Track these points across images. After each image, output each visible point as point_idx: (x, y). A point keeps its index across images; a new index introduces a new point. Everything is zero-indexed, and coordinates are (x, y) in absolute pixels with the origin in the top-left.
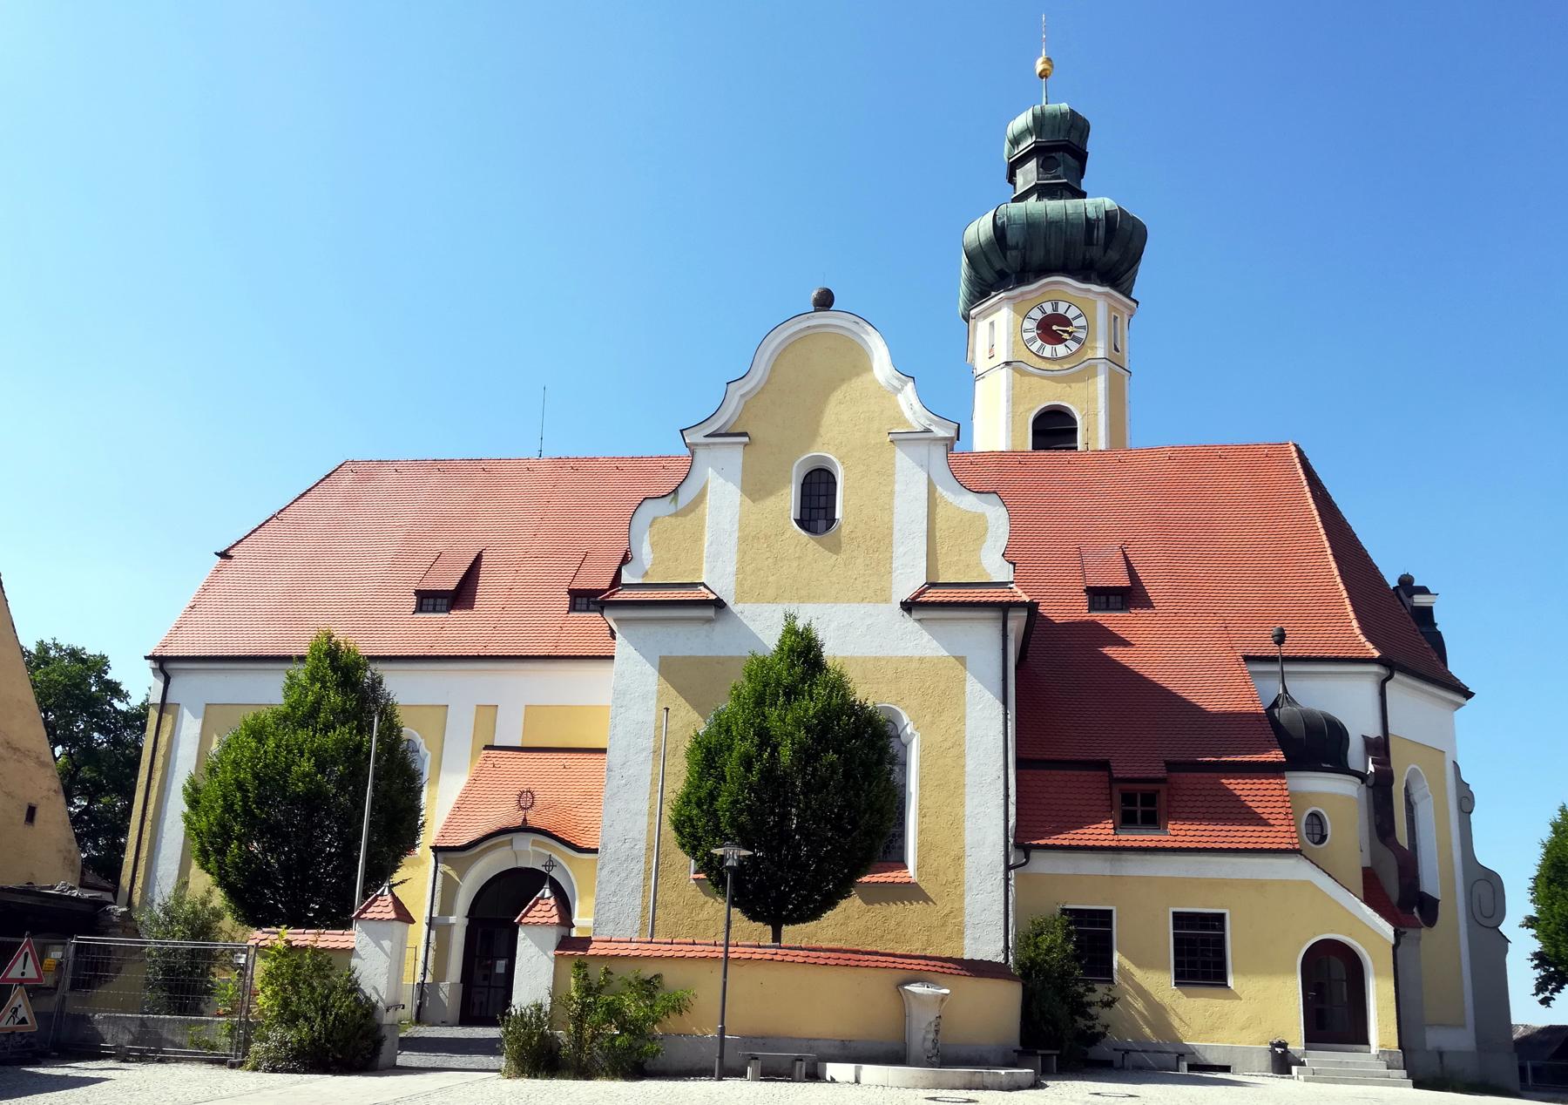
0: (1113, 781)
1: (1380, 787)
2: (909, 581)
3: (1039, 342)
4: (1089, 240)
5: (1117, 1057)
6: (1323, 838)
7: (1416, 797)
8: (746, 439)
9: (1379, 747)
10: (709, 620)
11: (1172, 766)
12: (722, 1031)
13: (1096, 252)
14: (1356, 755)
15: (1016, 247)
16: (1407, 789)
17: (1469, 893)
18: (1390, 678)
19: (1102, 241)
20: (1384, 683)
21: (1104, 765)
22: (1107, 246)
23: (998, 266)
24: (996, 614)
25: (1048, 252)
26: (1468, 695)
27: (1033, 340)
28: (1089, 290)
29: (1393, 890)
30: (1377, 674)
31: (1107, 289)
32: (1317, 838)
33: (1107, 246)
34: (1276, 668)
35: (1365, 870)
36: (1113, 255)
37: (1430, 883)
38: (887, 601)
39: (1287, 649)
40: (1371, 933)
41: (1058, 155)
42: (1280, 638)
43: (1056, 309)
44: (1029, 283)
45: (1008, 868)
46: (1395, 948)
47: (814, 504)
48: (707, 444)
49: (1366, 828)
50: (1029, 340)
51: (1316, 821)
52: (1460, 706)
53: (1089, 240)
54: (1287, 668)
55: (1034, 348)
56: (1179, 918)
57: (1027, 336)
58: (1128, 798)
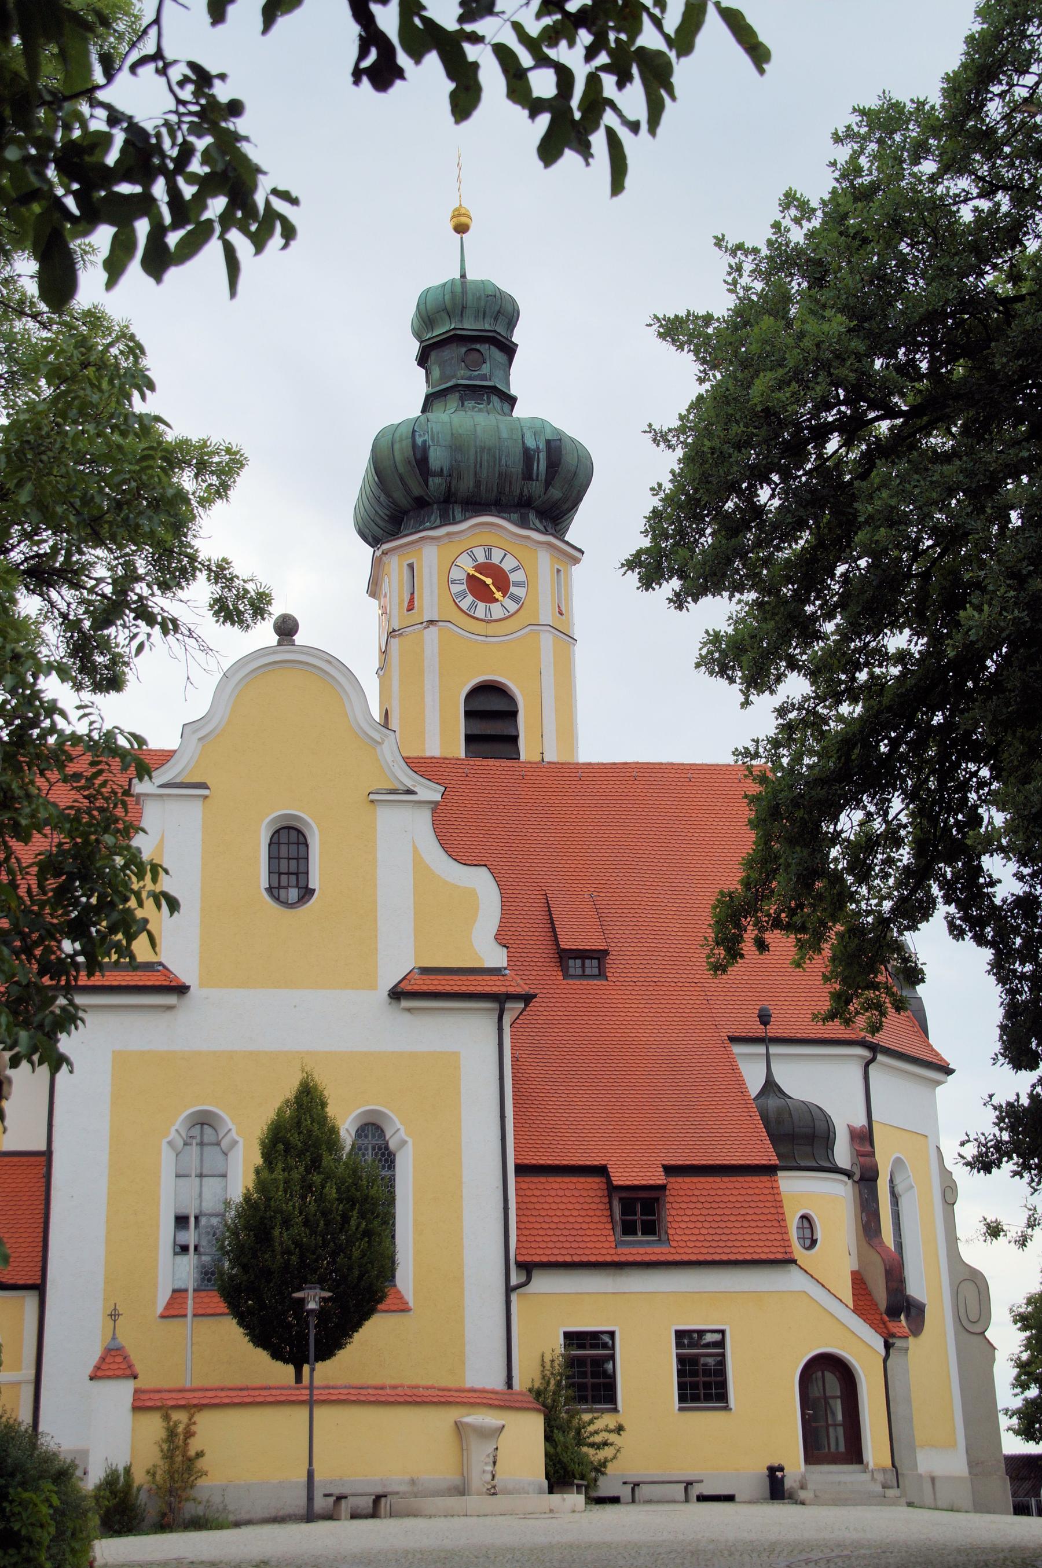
0: (612, 1189)
1: (865, 1178)
2: (395, 965)
3: (470, 598)
4: (528, 475)
5: (625, 1492)
6: (814, 1242)
7: (900, 1189)
8: (205, 792)
9: (864, 1138)
10: (170, 1008)
11: (670, 1170)
12: (310, 1474)
13: (536, 488)
14: (842, 1153)
15: (440, 473)
16: (891, 1181)
17: (956, 1294)
18: (873, 1060)
19: (543, 475)
20: (867, 1065)
21: (601, 1171)
22: (548, 483)
23: (417, 491)
24: (495, 1005)
25: (478, 484)
26: (949, 1071)
27: (462, 595)
28: (528, 537)
29: (881, 1295)
30: (861, 1057)
31: (550, 539)
32: (808, 1242)
33: (548, 483)
34: (761, 1049)
35: (853, 1273)
36: (555, 493)
37: (915, 1289)
38: (373, 987)
39: (773, 1030)
40: (860, 1345)
41: (483, 348)
42: (764, 1018)
43: (489, 556)
44: (456, 522)
45: (509, 1290)
46: (885, 1361)
47: (284, 869)
48: (161, 796)
49: (855, 1237)
50: (454, 582)
51: (806, 1224)
52: (939, 1083)
53: (528, 475)
54: (774, 1050)
55: (465, 604)
56: (680, 1334)
57: (456, 589)
58: (627, 1208)
